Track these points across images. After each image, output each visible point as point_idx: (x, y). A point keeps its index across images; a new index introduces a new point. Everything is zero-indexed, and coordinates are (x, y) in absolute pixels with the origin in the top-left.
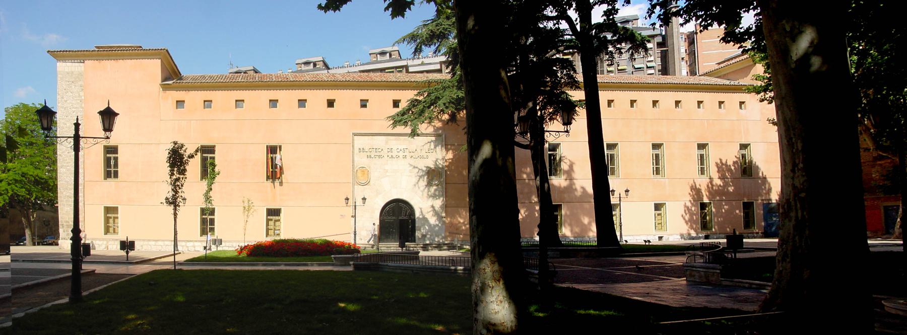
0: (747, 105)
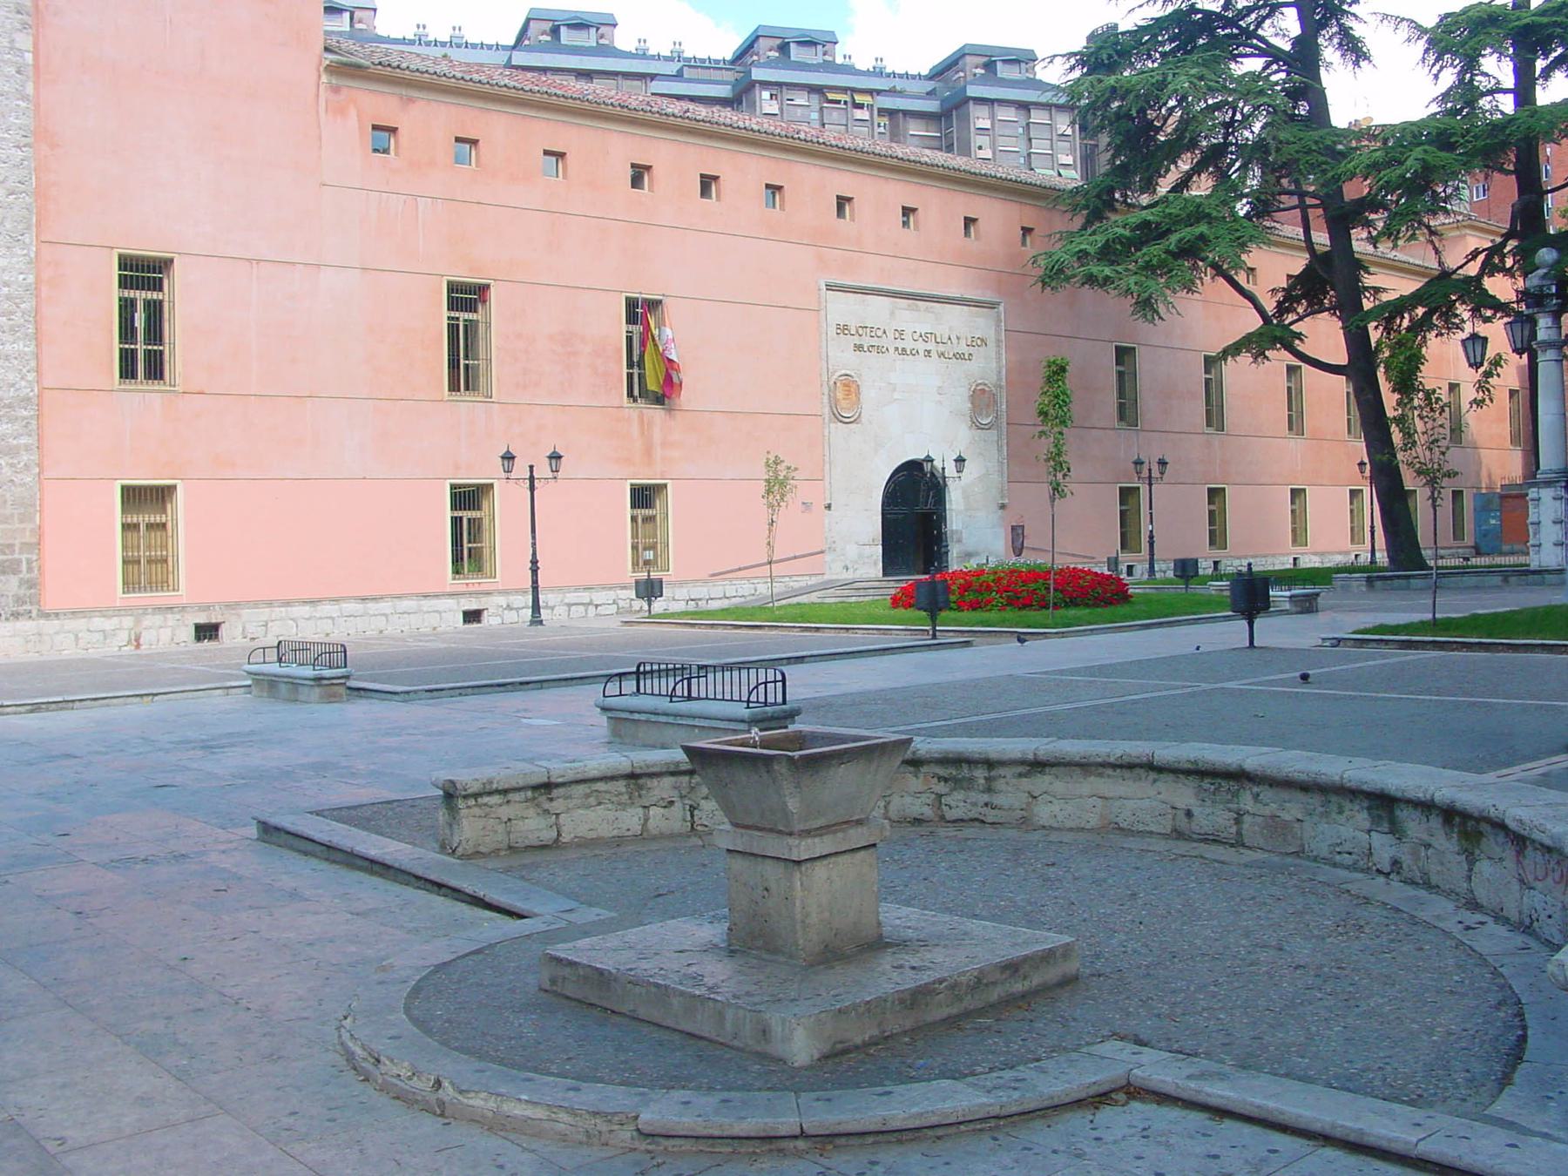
0: (856, 205)
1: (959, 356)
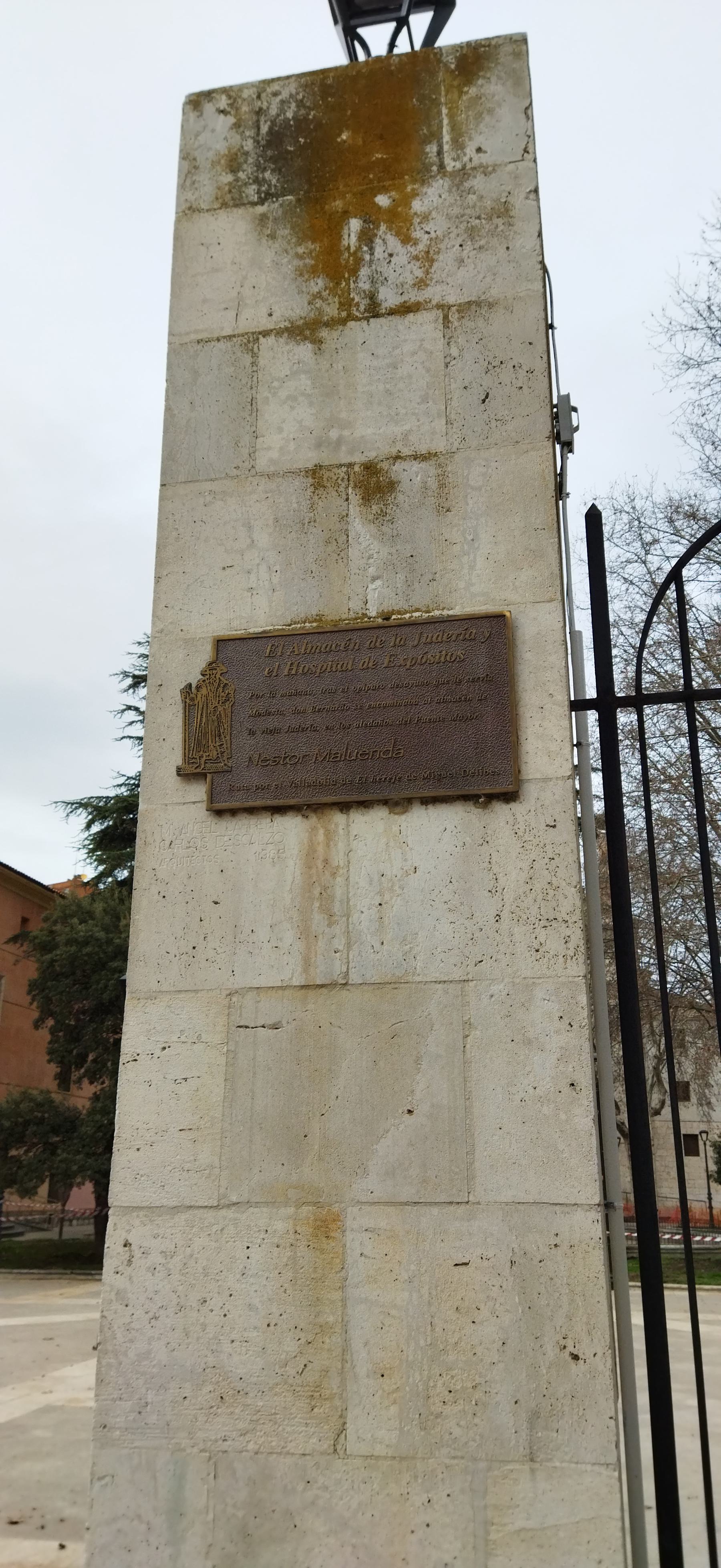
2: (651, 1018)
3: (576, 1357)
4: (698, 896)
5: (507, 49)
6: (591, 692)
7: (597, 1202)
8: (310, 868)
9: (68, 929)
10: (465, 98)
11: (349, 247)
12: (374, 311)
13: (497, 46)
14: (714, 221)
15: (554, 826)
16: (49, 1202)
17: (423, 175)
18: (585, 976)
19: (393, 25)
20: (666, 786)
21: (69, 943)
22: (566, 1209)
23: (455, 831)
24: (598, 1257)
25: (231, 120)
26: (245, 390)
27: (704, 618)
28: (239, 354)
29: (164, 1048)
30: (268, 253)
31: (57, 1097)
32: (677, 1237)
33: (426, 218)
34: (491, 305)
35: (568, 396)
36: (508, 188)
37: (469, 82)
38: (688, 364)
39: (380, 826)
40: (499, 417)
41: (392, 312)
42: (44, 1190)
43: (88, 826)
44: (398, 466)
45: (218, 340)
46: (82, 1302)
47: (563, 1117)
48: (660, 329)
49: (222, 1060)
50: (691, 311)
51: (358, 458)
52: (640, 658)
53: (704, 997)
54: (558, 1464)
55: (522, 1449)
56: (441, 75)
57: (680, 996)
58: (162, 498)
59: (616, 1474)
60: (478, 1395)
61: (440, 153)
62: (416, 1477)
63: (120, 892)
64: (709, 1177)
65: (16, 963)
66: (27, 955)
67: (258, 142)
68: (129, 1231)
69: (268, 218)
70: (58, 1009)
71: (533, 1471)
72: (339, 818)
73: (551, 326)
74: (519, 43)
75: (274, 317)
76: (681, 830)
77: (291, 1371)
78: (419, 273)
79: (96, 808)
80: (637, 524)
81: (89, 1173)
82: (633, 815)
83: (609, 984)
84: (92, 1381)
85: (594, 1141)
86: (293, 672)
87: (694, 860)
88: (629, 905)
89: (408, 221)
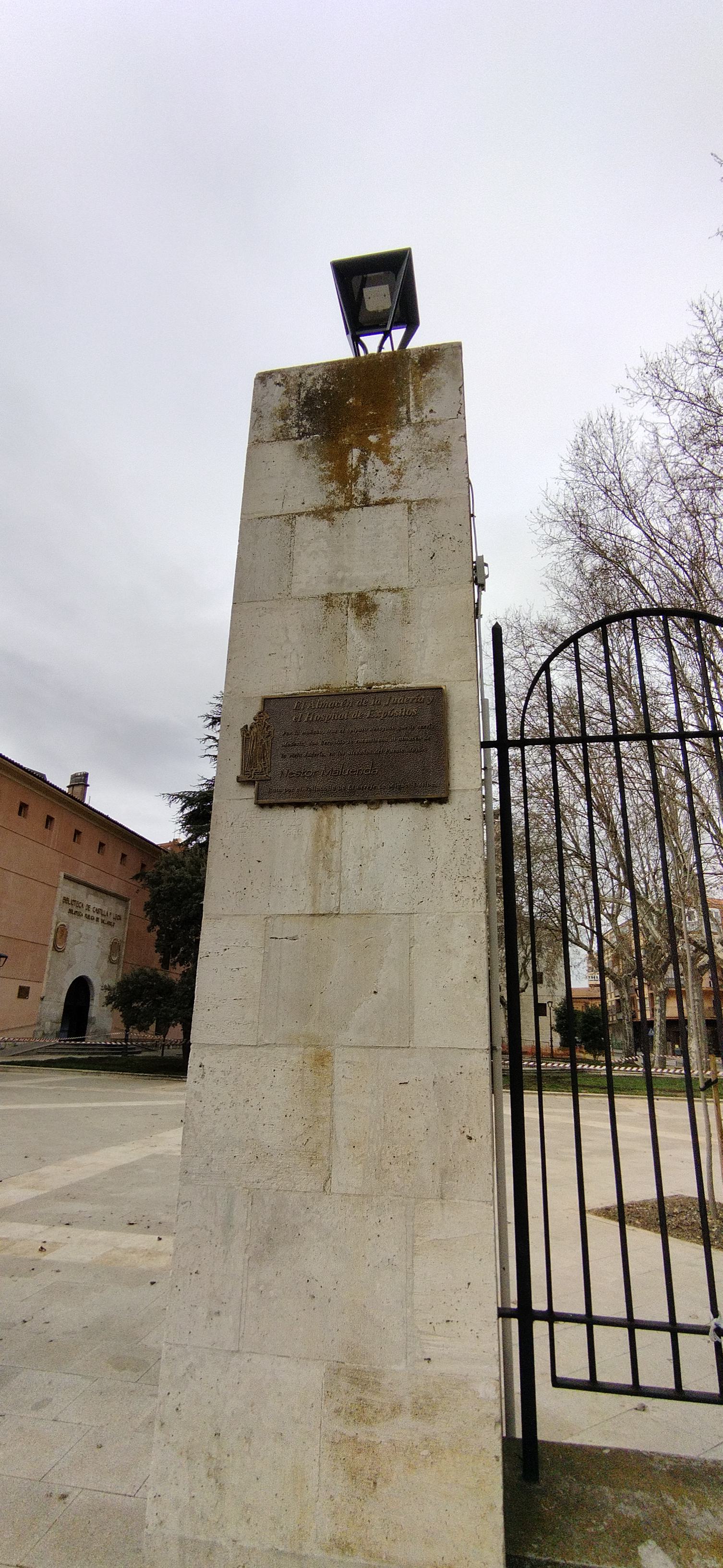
1: (109, 923)
2: (523, 934)
3: (470, 1138)
4: (553, 861)
5: (450, 351)
6: (493, 737)
7: (487, 1047)
8: (318, 842)
9: (168, 872)
10: (423, 380)
11: (352, 465)
12: (366, 502)
13: (443, 350)
14: (568, 459)
15: (469, 820)
16: (156, 1034)
17: (398, 425)
18: (485, 912)
19: (381, 336)
20: (535, 794)
21: (169, 880)
22: (468, 1052)
23: (408, 820)
24: (487, 1079)
25: (283, 389)
26: (286, 547)
27: (560, 693)
28: (283, 526)
29: (225, 950)
30: (304, 467)
31: (161, 973)
32: (531, 1063)
33: (398, 450)
34: (437, 502)
35: (482, 556)
36: (448, 434)
37: (426, 371)
38: (553, 541)
39: (362, 817)
40: (440, 568)
41: (377, 504)
42: (153, 1027)
43: (182, 809)
44: (379, 595)
45: (271, 517)
46: (176, 1093)
47: (469, 997)
48: (536, 521)
49: (261, 958)
50: (554, 510)
51: (355, 590)
52: (523, 717)
53: (553, 922)
54: (457, 1201)
55: (436, 1191)
56: (410, 366)
57: (540, 921)
58: (233, 611)
59: (492, 1207)
60: (412, 1159)
61: (408, 412)
62: (372, 1207)
63: (201, 850)
64: (552, 1028)
65: (138, 891)
66: (144, 887)
67: (299, 403)
68: (203, 1058)
69: (304, 447)
70: (162, 920)
71: (442, 1205)
72: (336, 811)
73: (472, 515)
74: (456, 348)
75: (305, 505)
76: (543, 821)
77: (299, 1143)
78: (394, 482)
79: (188, 798)
80: (521, 634)
81: (180, 1018)
82: (517, 812)
83: (498, 913)
84: (179, 1140)
85: (487, 1012)
86: (311, 719)
87: (552, 839)
88: (513, 866)
89: (388, 451)
